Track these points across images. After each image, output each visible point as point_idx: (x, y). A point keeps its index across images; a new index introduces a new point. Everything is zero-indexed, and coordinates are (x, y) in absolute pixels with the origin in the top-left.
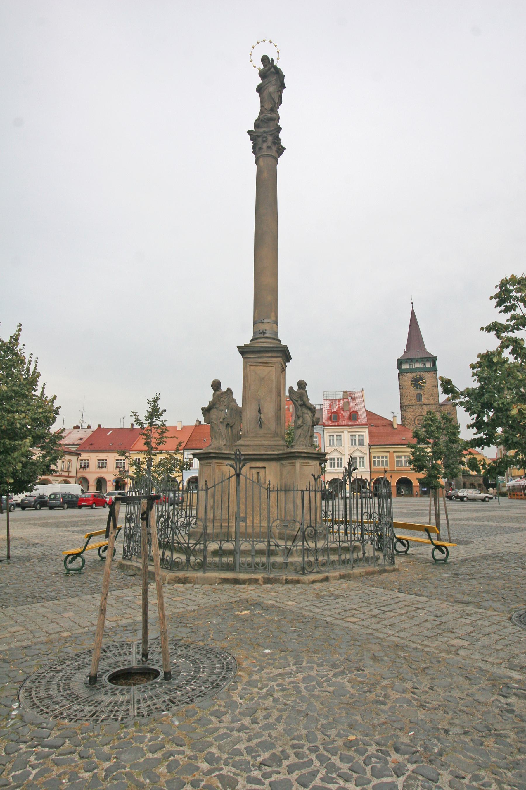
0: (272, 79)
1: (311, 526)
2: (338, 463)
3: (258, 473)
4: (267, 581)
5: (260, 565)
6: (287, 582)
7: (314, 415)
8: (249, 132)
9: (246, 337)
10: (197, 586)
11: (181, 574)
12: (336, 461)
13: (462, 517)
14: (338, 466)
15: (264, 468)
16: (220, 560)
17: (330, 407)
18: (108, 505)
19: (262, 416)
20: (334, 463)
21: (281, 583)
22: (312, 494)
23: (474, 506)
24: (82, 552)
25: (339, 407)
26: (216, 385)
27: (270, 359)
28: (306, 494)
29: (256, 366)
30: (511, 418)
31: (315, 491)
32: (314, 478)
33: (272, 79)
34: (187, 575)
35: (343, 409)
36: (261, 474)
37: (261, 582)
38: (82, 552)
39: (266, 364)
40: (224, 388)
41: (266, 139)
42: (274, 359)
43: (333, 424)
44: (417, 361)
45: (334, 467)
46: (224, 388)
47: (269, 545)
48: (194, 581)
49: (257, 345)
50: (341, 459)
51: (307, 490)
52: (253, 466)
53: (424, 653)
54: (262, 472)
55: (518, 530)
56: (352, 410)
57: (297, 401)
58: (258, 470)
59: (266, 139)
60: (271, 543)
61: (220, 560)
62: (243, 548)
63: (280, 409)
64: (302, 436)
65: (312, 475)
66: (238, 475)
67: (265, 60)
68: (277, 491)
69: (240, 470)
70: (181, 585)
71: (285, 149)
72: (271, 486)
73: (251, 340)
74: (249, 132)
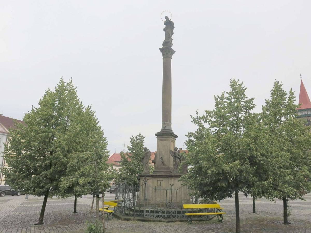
1: (169, 203)
3: (161, 182)
5: (184, 216)
9: (159, 129)
21: (122, 220)
24: (108, 208)
27: (166, 138)
28: (168, 191)
29: (162, 141)
32: (171, 185)
33: (169, 26)
36: (161, 183)
38: (108, 208)
39: (165, 140)
41: (167, 50)
42: (168, 138)
44: (305, 110)
46: (294, 102)
51: (168, 190)
52: (159, 179)
53: (64, 228)
54: (162, 182)
55: (308, 208)
58: (161, 181)
59: (167, 50)
60: (156, 208)
63: (170, 157)
64: (175, 168)
66: (145, 184)
67: (167, 18)
69: (146, 182)
71: (175, 51)
72: (156, 188)
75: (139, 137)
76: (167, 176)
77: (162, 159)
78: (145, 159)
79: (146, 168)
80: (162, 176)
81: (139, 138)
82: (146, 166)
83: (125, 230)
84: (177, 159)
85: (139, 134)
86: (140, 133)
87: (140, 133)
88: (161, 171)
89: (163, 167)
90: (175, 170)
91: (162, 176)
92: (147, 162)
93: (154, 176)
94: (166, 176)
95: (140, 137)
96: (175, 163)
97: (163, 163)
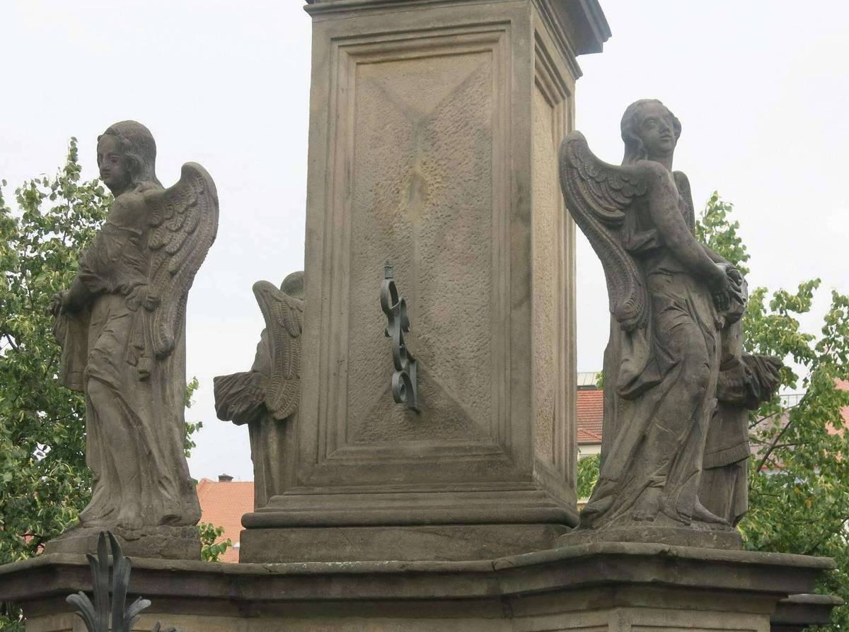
64: (652, 452)
75: (61, 201)
76: (507, 588)
77: (393, 307)
78: (110, 306)
79: (125, 461)
80: (408, 591)
81: (57, 210)
82: (130, 419)
83: (404, 233)
84: (677, 290)
85: (64, 162)
86: (73, 157)
87: (73, 157)
88: (382, 507)
89: (417, 446)
90: (652, 472)
91: (408, 591)
92: (146, 364)
93: (278, 592)
94: (480, 589)
95: (68, 194)
96: (654, 361)
97: (413, 400)
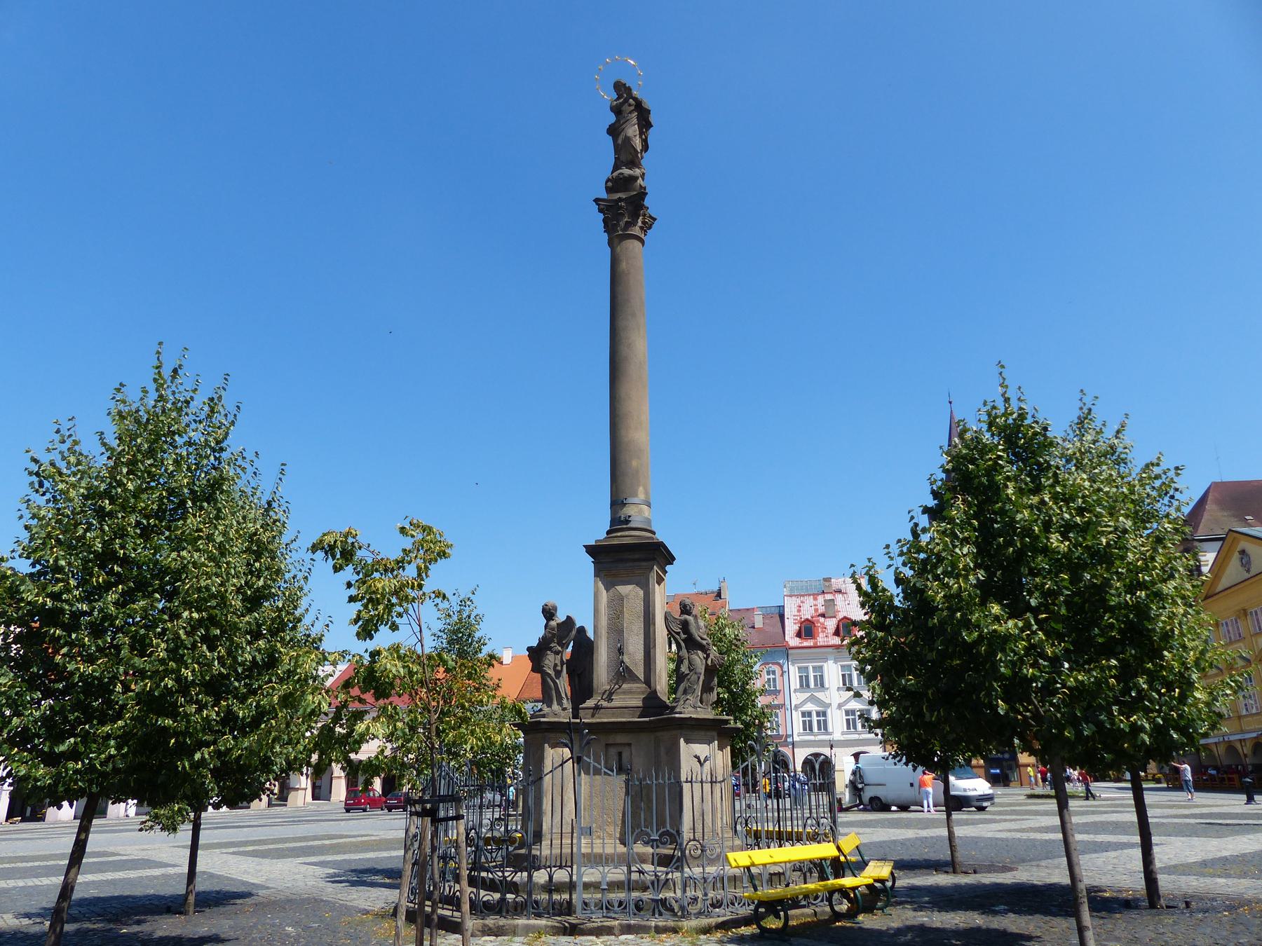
0: (629, 109)
2: (819, 722)
3: (620, 754)
4: (628, 929)
5: (616, 905)
6: (659, 930)
7: (708, 656)
8: (597, 200)
10: (516, 939)
11: (491, 921)
12: (815, 719)
13: (1037, 825)
14: (819, 728)
15: (630, 745)
16: (550, 897)
17: (799, 611)
18: (323, 548)
19: (626, 659)
20: (810, 722)
22: (697, 786)
23: (1166, 798)
25: (816, 610)
26: (549, 613)
30: (408, 801)
31: (702, 782)
34: (501, 923)
35: (823, 615)
37: (616, 932)
40: (561, 617)
43: (805, 644)
45: (811, 729)
47: (630, 872)
48: (514, 932)
49: (615, 542)
50: (824, 714)
56: (841, 616)
57: (678, 633)
58: (620, 749)
60: (633, 869)
61: (550, 897)
62: (585, 879)
65: (696, 757)
67: (621, 88)
68: (702, 782)
70: (492, 938)
73: (608, 533)
74: (597, 200)
